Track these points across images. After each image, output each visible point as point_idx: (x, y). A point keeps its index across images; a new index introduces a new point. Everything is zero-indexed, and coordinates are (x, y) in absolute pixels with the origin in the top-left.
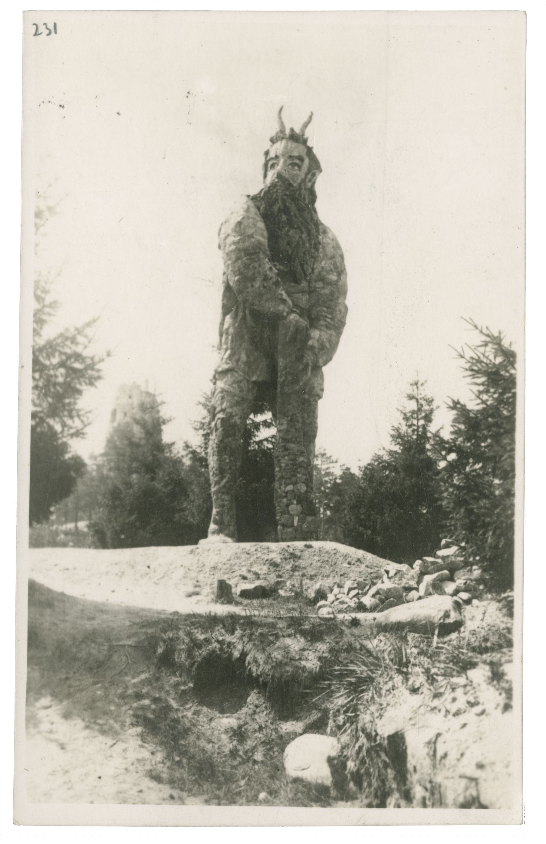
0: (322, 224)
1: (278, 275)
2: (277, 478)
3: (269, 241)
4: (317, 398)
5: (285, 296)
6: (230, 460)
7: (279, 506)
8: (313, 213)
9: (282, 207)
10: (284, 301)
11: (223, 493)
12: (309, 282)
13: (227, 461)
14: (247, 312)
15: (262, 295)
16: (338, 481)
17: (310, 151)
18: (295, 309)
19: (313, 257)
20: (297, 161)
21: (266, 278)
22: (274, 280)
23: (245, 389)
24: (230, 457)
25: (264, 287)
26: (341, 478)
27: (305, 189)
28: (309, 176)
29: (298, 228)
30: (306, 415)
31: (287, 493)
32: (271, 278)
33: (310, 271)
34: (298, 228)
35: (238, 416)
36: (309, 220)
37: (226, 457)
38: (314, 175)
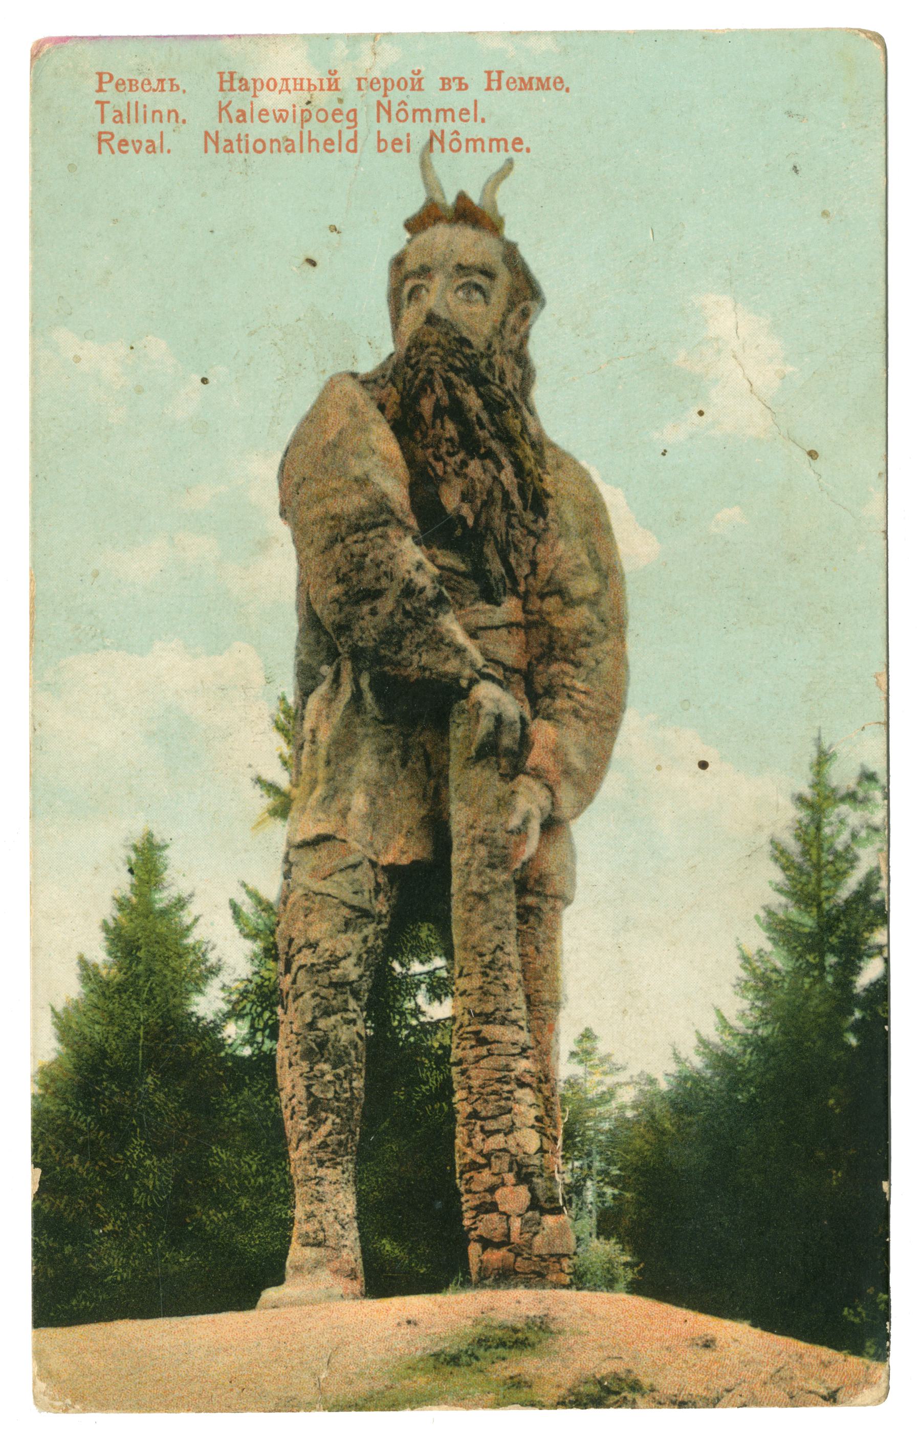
0: (553, 446)
1: (440, 580)
2: (460, 1118)
3: (412, 494)
4: (559, 904)
5: (461, 638)
6: (337, 1076)
7: (469, 1191)
8: (526, 414)
9: (445, 401)
10: (460, 651)
11: (321, 1163)
12: (524, 598)
13: (329, 1077)
14: (365, 682)
15: (402, 634)
16: (630, 1114)
17: (511, 253)
18: (489, 671)
19: (531, 533)
20: (478, 279)
21: (409, 591)
22: (430, 593)
23: (369, 886)
24: (334, 1067)
25: (407, 614)
26: (635, 1107)
27: (503, 353)
28: (512, 318)
29: (490, 454)
30: (530, 949)
31: (487, 1156)
32: (422, 590)
33: (526, 569)
34: (490, 454)
35: (352, 960)
36: (517, 435)
37: (326, 1067)
38: (525, 315)
